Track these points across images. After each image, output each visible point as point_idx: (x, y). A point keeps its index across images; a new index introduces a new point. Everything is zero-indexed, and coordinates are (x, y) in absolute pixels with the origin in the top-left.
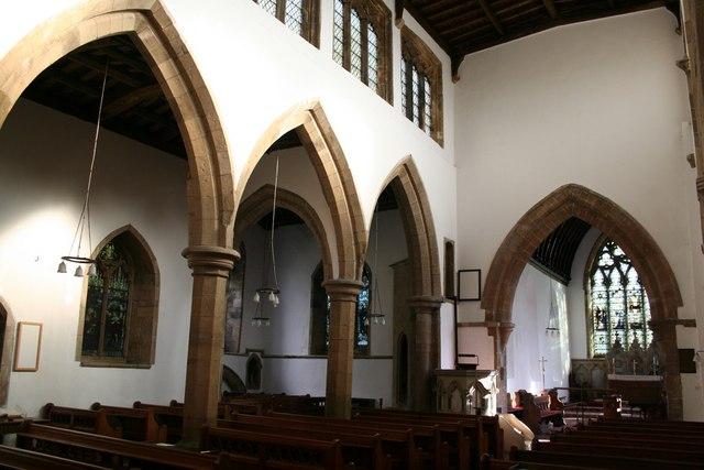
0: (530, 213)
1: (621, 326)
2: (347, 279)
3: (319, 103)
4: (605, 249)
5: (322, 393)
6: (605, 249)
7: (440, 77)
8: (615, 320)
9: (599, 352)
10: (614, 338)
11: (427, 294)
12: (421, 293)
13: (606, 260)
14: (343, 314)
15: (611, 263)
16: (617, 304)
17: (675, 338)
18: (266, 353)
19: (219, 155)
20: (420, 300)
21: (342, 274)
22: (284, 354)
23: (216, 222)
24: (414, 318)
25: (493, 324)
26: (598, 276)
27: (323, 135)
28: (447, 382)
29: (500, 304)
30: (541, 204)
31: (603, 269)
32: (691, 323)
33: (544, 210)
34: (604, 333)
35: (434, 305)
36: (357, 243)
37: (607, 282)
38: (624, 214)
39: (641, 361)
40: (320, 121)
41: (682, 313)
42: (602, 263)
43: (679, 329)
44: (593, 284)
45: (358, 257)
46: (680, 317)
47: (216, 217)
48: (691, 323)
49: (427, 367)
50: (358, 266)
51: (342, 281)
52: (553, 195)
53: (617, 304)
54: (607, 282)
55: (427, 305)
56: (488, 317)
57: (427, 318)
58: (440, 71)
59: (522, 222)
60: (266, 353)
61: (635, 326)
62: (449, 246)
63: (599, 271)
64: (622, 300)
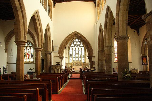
0: (68, 36)
1: (74, 57)
2: (40, 47)
3: (38, 11)
4: (72, 43)
5: (16, 71)
6: (72, 43)
7: (52, 7)
8: (73, 56)
9: (70, 62)
10: (73, 60)
11: (49, 51)
12: (48, 50)
13: (72, 45)
14: (39, 54)
15: (73, 45)
16: (74, 53)
17: (92, 59)
18: (8, 63)
19: (25, 20)
20: (48, 52)
21: (39, 46)
22: (10, 63)
23: (23, 35)
24: (46, 55)
25: (60, 56)
26: (71, 48)
27: (38, 18)
28: (54, 68)
29: (62, 53)
30: (70, 34)
31: (72, 46)
32: (95, 57)
33: (71, 35)
34: (72, 58)
35: (50, 53)
36: (42, 40)
37: (72, 49)
38: (85, 38)
39: (78, 63)
40: (118, 27)
41: (93, 55)
42: (71, 46)
43: (93, 58)
44: (70, 49)
45: (42, 43)
46: (93, 56)
47: (24, 34)
48: (95, 57)
49: (49, 65)
50: (42, 45)
51: (39, 48)
52: (73, 33)
53: (74, 53)
54: (72, 49)
55: (49, 53)
56: (59, 55)
57: (49, 55)
58: (52, 5)
59: (66, 38)
60: (8, 63)
61: (77, 57)
62: (52, 41)
63: (71, 47)
64: (75, 52)
